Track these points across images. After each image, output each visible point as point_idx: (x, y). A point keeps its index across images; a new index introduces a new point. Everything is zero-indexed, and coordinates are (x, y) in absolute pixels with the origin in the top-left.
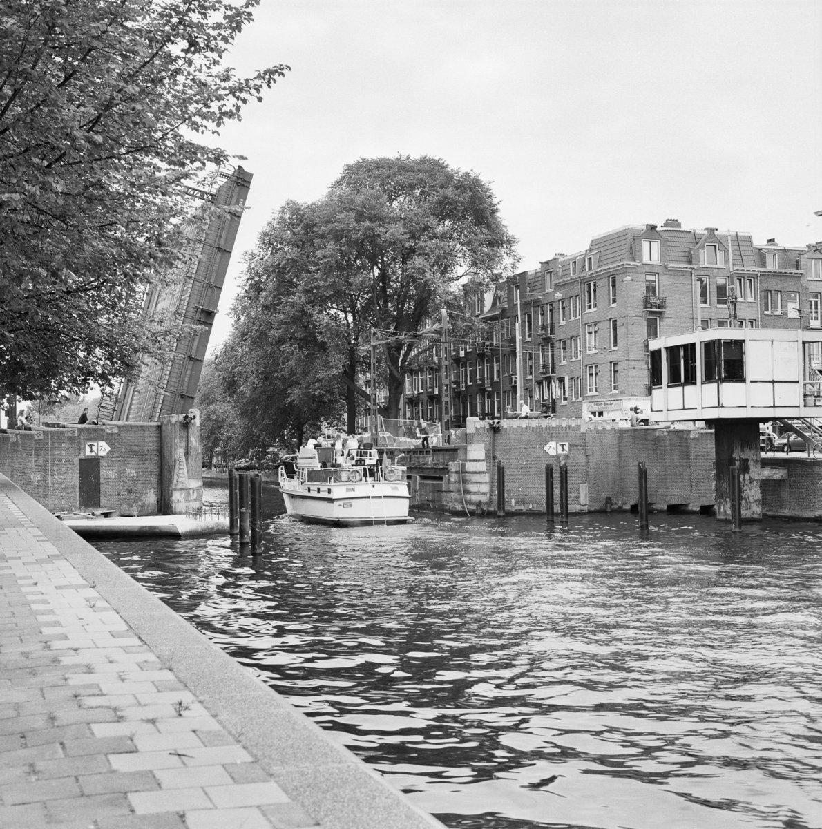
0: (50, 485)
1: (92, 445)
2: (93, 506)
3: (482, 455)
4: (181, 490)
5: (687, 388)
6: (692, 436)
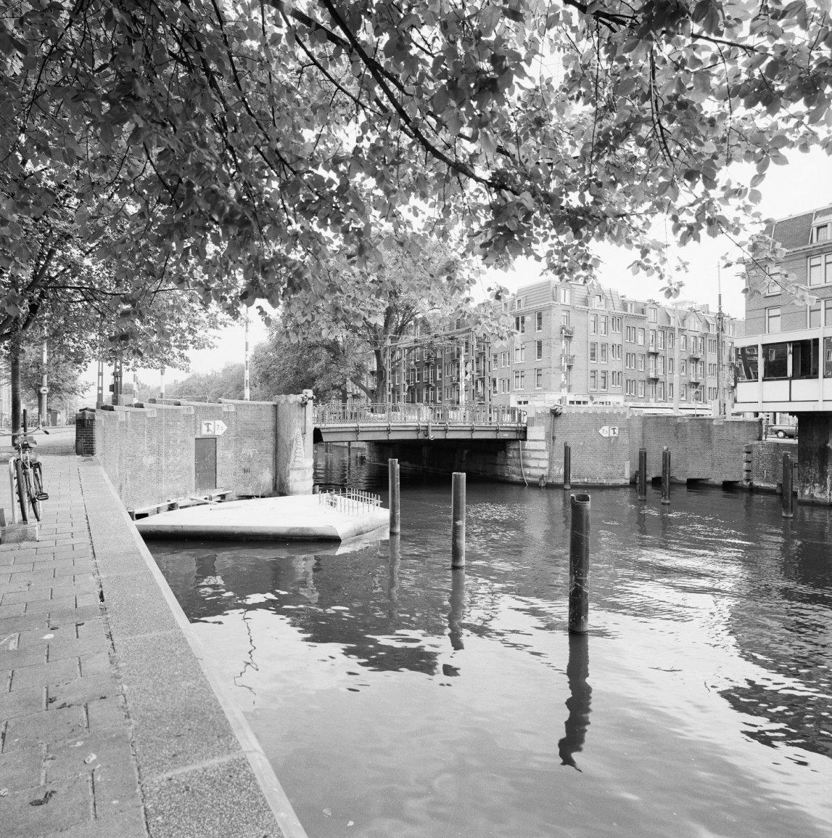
0: (164, 467)
1: (208, 424)
2: (209, 487)
3: (542, 436)
4: (299, 469)
5: (793, 382)
6: (714, 423)
